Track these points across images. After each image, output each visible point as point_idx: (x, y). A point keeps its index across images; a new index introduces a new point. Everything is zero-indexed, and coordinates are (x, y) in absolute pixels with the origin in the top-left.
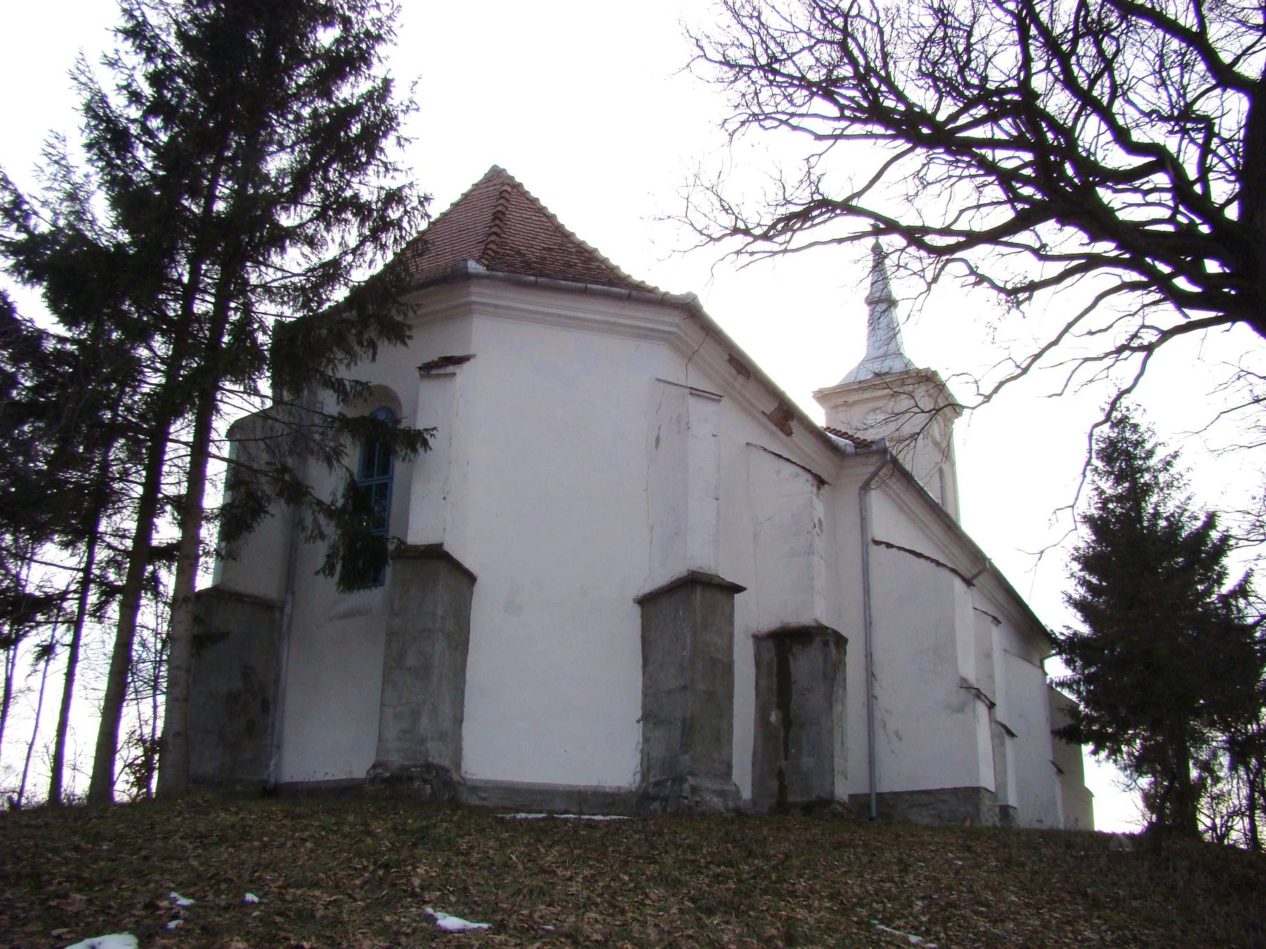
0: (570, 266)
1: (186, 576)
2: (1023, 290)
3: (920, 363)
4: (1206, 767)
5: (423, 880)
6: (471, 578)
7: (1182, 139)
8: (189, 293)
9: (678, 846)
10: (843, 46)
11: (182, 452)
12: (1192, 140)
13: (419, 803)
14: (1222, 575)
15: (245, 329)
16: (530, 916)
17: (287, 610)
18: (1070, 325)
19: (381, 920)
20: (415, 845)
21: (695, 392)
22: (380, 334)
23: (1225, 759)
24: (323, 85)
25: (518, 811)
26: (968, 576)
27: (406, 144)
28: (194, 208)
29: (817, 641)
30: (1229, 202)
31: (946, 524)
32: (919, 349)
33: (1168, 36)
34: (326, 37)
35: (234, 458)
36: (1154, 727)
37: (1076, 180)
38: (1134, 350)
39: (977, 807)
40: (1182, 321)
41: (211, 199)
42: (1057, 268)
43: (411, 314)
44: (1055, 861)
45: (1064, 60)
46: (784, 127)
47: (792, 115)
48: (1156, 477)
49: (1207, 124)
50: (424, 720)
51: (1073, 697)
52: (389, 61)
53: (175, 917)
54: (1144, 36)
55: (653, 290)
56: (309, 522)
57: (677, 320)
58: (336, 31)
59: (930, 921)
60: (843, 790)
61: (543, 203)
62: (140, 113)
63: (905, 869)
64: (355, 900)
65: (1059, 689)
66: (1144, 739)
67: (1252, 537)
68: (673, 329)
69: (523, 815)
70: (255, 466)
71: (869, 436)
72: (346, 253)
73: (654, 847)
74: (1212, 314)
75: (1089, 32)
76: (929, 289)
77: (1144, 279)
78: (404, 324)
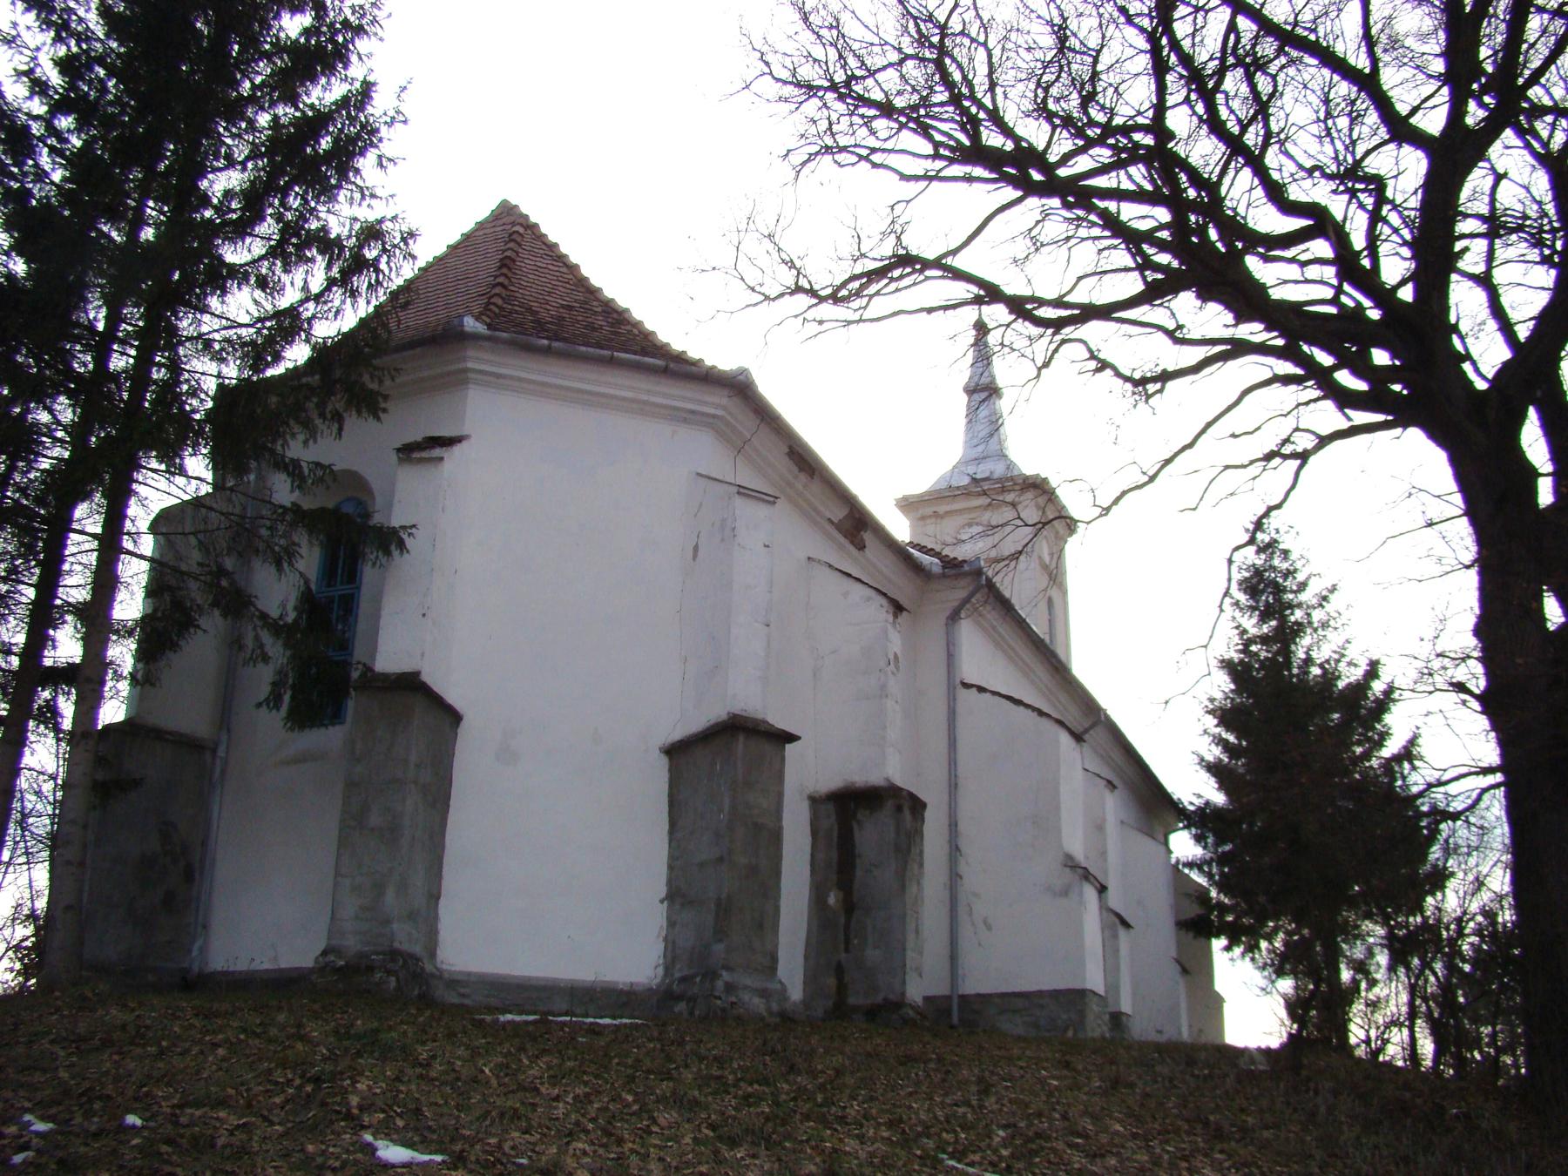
0: (594, 329)
1: (89, 704)
2: (1154, 380)
3: (1028, 470)
4: (1361, 967)
5: (363, 1099)
6: (454, 717)
7: (1349, 202)
8: (102, 346)
9: (701, 1059)
10: (940, 66)
11: (87, 546)
12: (1361, 206)
13: (382, 997)
14: (1384, 736)
15: (170, 393)
16: (499, 1146)
17: (221, 752)
18: (1209, 425)
19: (303, 1150)
20: (359, 1054)
21: (744, 492)
22: (349, 404)
23: (1382, 958)
24: (287, 85)
25: (505, 1011)
26: (1078, 729)
27: (390, 166)
28: (114, 234)
29: (890, 804)
30: (1403, 283)
31: (1052, 664)
32: (1027, 452)
33: (1336, 78)
34: (293, 25)
35: (157, 556)
36: (1299, 919)
37: (1219, 245)
38: (1285, 457)
39: (1082, 1014)
40: (1344, 425)
41: (139, 221)
42: (1197, 354)
43: (388, 383)
44: (1171, 1080)
45: (1208, 98)
46: (864, 165)
47: (874, 150)
48: (1309, 615)
49: (1377, 185)
50: (390, 897)
51: (1201, 880)
52: (376, 60)
53: (25, 1147)
54: (1307, 77)
55: (697, 363)
56: (249, 642)
57: (725, 401)
58: (306, 20)
59: (1012, 1156)
60: (916, 991)
61: (564, 249)
62: (45, 108)
63: (985, 1091)
64: (272, 1124)
65: (1186, 871)
66: (1289, 933)
67: (1420, 687)
68: (720, 412)
69: (509, 1017)
70: (184, 567)
71: (962, 552)
72: (307, 300)
73: (669, 1059)
74: (1380, 418)
75: (1240, 62)
76: (1038, 376)
77: (1299, 371)
78: (378, 393)
